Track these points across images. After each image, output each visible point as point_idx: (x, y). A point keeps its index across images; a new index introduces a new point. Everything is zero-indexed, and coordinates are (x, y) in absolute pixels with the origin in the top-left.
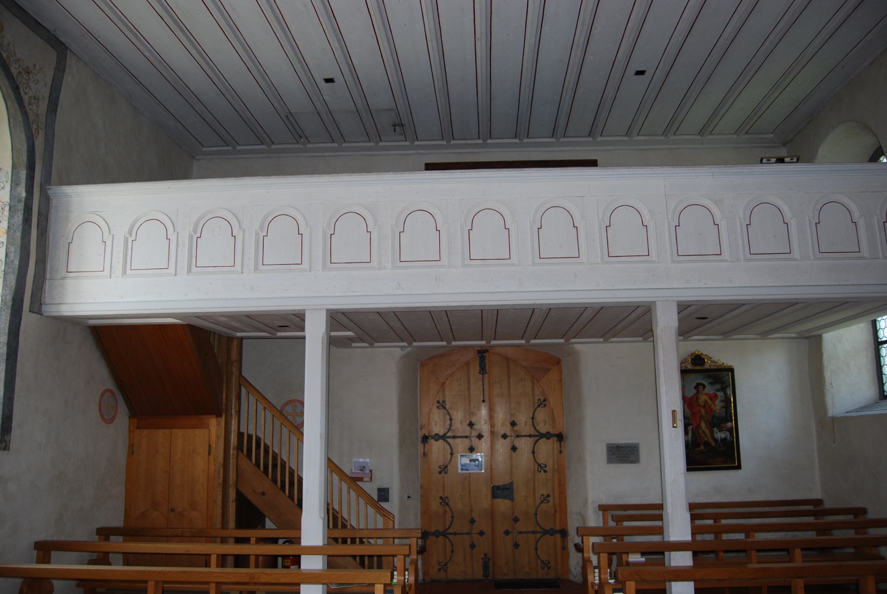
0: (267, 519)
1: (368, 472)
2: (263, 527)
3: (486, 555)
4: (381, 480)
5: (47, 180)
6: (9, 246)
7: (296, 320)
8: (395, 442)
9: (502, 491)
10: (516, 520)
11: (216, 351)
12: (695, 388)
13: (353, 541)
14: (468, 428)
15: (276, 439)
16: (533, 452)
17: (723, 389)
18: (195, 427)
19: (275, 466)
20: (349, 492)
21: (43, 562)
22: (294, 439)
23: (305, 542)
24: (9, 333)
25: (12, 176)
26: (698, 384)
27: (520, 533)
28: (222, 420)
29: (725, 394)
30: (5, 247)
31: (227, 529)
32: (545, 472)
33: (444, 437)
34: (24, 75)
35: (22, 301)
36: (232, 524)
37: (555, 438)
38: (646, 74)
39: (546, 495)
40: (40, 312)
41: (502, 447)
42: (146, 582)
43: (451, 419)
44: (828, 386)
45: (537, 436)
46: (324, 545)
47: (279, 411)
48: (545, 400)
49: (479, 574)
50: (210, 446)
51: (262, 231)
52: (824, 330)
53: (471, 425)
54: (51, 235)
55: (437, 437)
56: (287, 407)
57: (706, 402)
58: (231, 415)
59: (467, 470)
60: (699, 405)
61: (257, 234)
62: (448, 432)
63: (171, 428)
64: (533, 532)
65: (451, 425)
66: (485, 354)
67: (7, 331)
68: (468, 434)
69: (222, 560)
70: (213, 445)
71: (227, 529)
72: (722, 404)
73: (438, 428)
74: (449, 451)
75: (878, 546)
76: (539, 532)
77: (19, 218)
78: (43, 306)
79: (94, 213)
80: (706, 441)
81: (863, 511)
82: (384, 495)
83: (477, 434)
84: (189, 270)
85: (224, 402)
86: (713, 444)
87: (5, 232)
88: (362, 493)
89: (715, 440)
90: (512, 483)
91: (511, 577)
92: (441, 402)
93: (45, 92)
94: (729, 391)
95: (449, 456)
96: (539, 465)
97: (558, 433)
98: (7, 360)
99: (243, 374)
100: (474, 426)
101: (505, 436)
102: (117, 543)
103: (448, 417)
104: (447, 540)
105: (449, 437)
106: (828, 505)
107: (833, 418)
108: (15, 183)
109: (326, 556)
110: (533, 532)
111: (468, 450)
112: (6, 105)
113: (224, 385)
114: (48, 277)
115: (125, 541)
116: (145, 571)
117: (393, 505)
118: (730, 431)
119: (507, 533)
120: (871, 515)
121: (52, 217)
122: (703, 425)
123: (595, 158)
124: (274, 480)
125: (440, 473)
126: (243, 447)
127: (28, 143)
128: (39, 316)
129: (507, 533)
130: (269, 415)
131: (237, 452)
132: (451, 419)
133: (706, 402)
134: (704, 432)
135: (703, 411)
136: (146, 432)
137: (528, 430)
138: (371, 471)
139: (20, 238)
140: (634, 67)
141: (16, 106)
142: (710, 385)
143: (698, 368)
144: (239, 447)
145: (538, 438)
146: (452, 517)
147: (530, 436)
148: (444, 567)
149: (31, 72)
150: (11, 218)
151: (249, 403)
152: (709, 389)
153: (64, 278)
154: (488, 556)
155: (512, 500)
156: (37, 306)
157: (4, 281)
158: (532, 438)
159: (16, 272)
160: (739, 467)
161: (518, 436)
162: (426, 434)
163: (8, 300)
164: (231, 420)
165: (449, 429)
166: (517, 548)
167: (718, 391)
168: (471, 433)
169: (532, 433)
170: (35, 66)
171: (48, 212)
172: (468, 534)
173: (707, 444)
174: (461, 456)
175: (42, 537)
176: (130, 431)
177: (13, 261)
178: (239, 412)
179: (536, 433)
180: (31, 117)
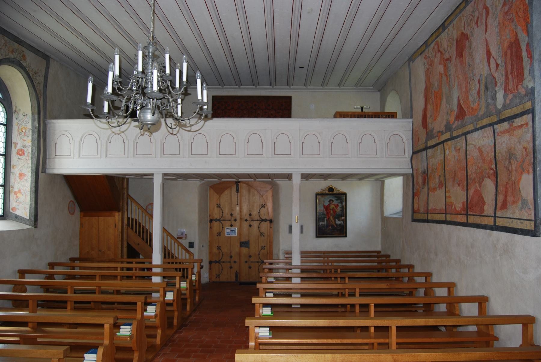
0: (140, 255)
1: (184, 235)
2: (139, 257)
3: (236, 271)
4: (190, 239)
5: (45, 117)
6: (33, 147)
7: (150, 177)
8: (197, 222)
9: (244, 244)
10: (250, 256)
11: (117, 184)
12: (329, 202)
13: (176, 263)
14: (230, 216)
15: (144, 220)
16: (259, 228)
17: (341, 202)
18: (109, 216)
19: (143, 232)
20: (174, 244)
21: (52, 269)
22: (151, 220)
23: (154, 263)
24: (35, 182)
25: (32, 117)
26: (330, 200)
27: (252, 262)
28: (121, 213)
29: (342, 204)
30: (31, 147)
31: (124, 258)
32: (264, 236)
33: (219, 220)
34: (35, 75)
35: (39, 169)
36: (125, 256)
37: (269, 222)
38: (305, 68)
39: (263, 246)
40: (45, 172)
41: (245, 225)
42: (96, 276)
43: (223, 212)
44: (385, 203)
45: (260, 220)
46: (161, 264)
47: (145, 210)
48: (265, 205)
49: (233, 279)
50: (115, 224)
51: (136, 141)
52: (386, 178)
53: (231, 215)
54: (48, 140)
55: (216, 220)
56: (149, 206)
57: (333, 208)
58: (124, 211)
59: (229, 235)
60: (330, 209)
61: (134, 142)
62: (221, 218)
63: (99, 217)
64: (258, 262)
65: (223, 215)
66: (238, 184)
67: (34, 181)
68: (230, 219)
69: (122, 269)
70: (117, 224)
71: (124, 258)
72: (340, 209)
73: (217, 216)
74: (222, 226)
75: (401, 268)
76: (260, 262)
77: (36, 135)
78: (46, 170)
79: (66, 131)
80: (332, 225)
81: (389, 256)
82: (191, 245)
83: (234, 219)
84: (106, 156)
85: (121, 206)
86: (335, 226)
87: (30, 141)
88: (180, 244)
89: (336, 224)
90: (249, 241)
91: (248, 281)
92: (218, 205)
93: (42, 79)
94: (344, 204)
95: (221, 228)
96: (261, 233)
97: (270, 219)
98: (35, 193)
99: (129, 194)
100: (233, 216)
101: (246, 220)
102: (77, 263)
103: (221, 211)
104: (220, 265)
105: (222, 220)
106: (382, 253)
107: (385, 217)
108: (33, 121)
109: (162, 269)
110: (258, 262)
111: (230, 226)
112: (28, 89)
113: (121, 200)
114: (47, 158)
115: (80, 262)
116: (95, 272)
117: (195, 251)
118: (343, 220)
119: (246, 262)
120: (391, 258)
121: (48, 132)
122: (331, 218)
123: (290, 95)
124: (143, 239)
125: (217, 236)
126: (129, 224)
127: (38, 104)
128: (45, 174)
129: (246, 262)
130: (140, 211)
131: (127, 227)
132: (223, 212)
133: (333, 208)
134: (332, 221)
135: (332, 212)
136: (87, 218)
137: (257, 217)
138: (186, 235)
139: (37, 143)
140: (298, 65)
141: (33, 89)
142: (336, 201)
143: (330, 193)
144: (128, 225)
145: (261, 221)
146: (222, 255)
147: (258, 220)
148: (218, 276)
149: (37, 72)
150: (33, 135)
151: (132, 207)
152: (335, 202)
153: (54, 158)
154: (237, 272)
155: (249, 248)
156: (44, 171)
157: (32, 161)
158: (258, 221)
159: (36, 157)
160: (346, 236)
161: (252, 220)
162: (212, 219)
163: (34, 169)
164: (124, 213)
165: (222, 217)
166: (250, 269)
167: (339, 203)
168: (231, 219)
169: (259, 219)
170: (38, 70)
171: (46, 130)
172: (229, 262)
173: (332, 226)
174: (227, 228)
175: (50, 261)
176: (81, 218)
177: (34, 153)
178: (127, 210)
179: (260, 219)
180: (38, 92)
